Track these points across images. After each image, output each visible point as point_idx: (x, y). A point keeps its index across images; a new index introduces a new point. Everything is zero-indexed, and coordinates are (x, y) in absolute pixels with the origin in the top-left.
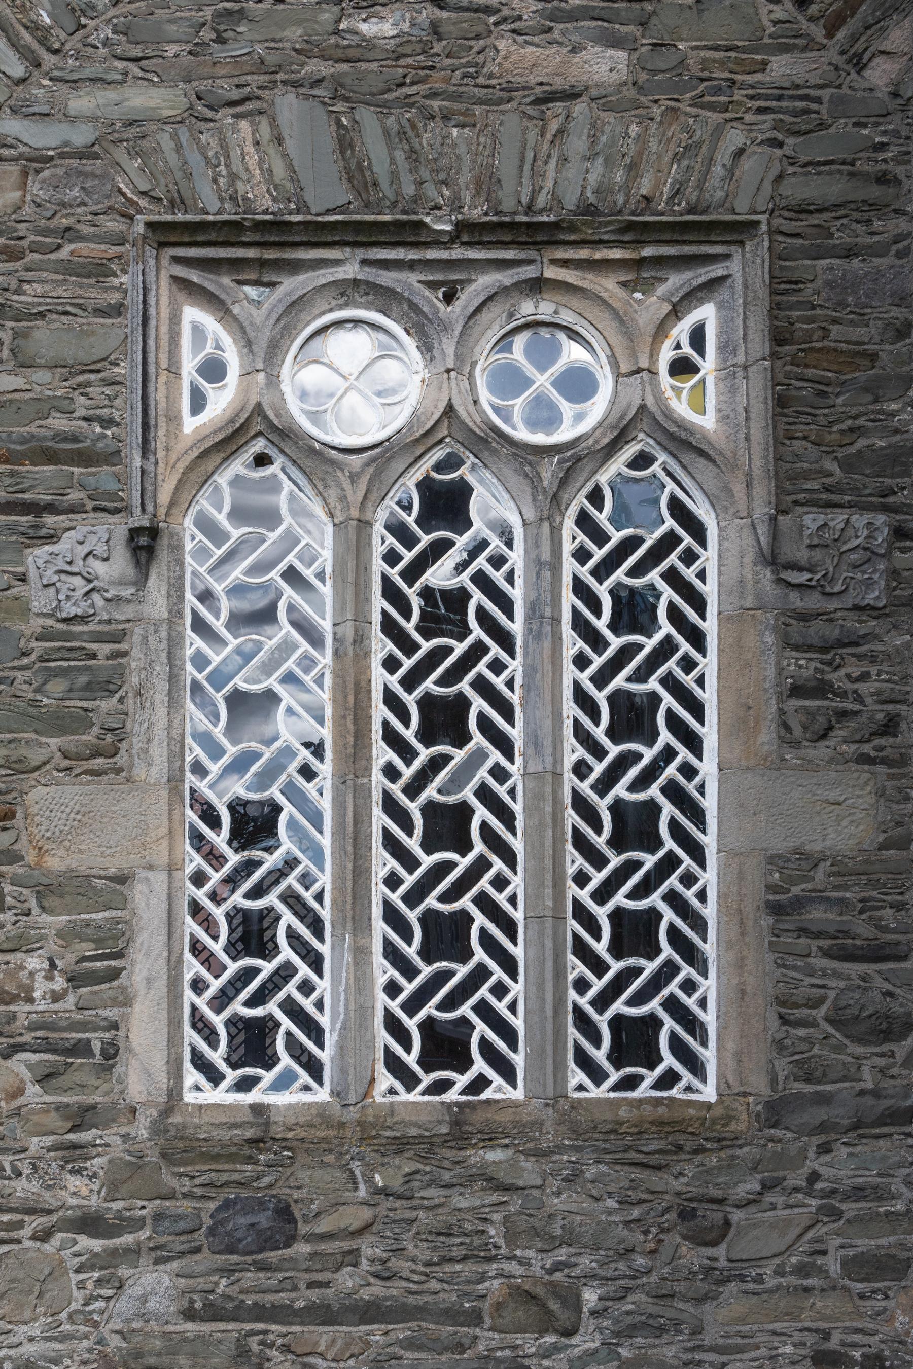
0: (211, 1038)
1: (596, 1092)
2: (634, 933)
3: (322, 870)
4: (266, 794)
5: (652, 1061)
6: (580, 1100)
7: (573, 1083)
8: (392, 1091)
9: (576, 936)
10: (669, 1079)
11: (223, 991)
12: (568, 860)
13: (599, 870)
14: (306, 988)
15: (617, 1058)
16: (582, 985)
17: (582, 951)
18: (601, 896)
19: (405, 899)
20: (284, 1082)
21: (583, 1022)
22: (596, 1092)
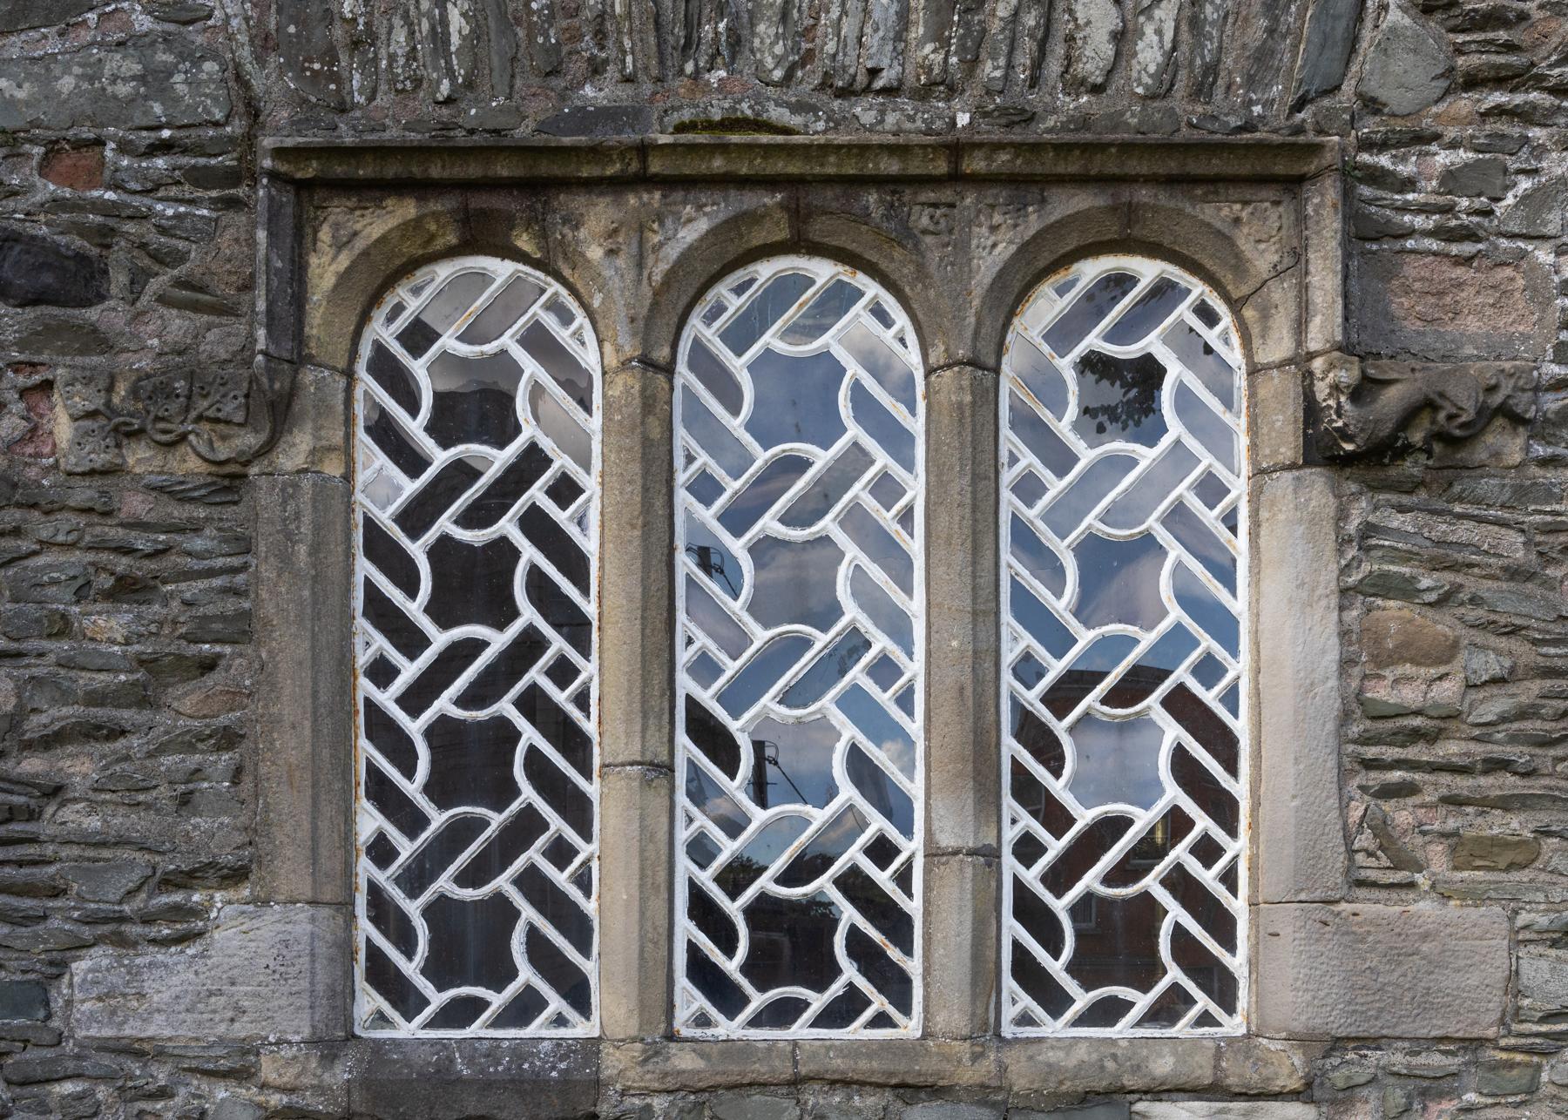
0: (1050, 935)
1: (407, 1030)
2: (473, 762)
3: (910, 655)
4: (814, 529)
5: (1146, 974)
6: (378, 1044)
7: (1009, 1013)
8: (381, 1019)
9: (372, 770)
10: (526, 1007)
11: (420, 858)
12: (358, 642)
13: (412, 657)
14: (1207, 851)
15: (761, 970)
16: (382, 852)
17: (384, 794)
18: (415, 700)
19: (1048, 699)
20: (844, 1010)
21: (1030, 911)
22: (407, 1030)
